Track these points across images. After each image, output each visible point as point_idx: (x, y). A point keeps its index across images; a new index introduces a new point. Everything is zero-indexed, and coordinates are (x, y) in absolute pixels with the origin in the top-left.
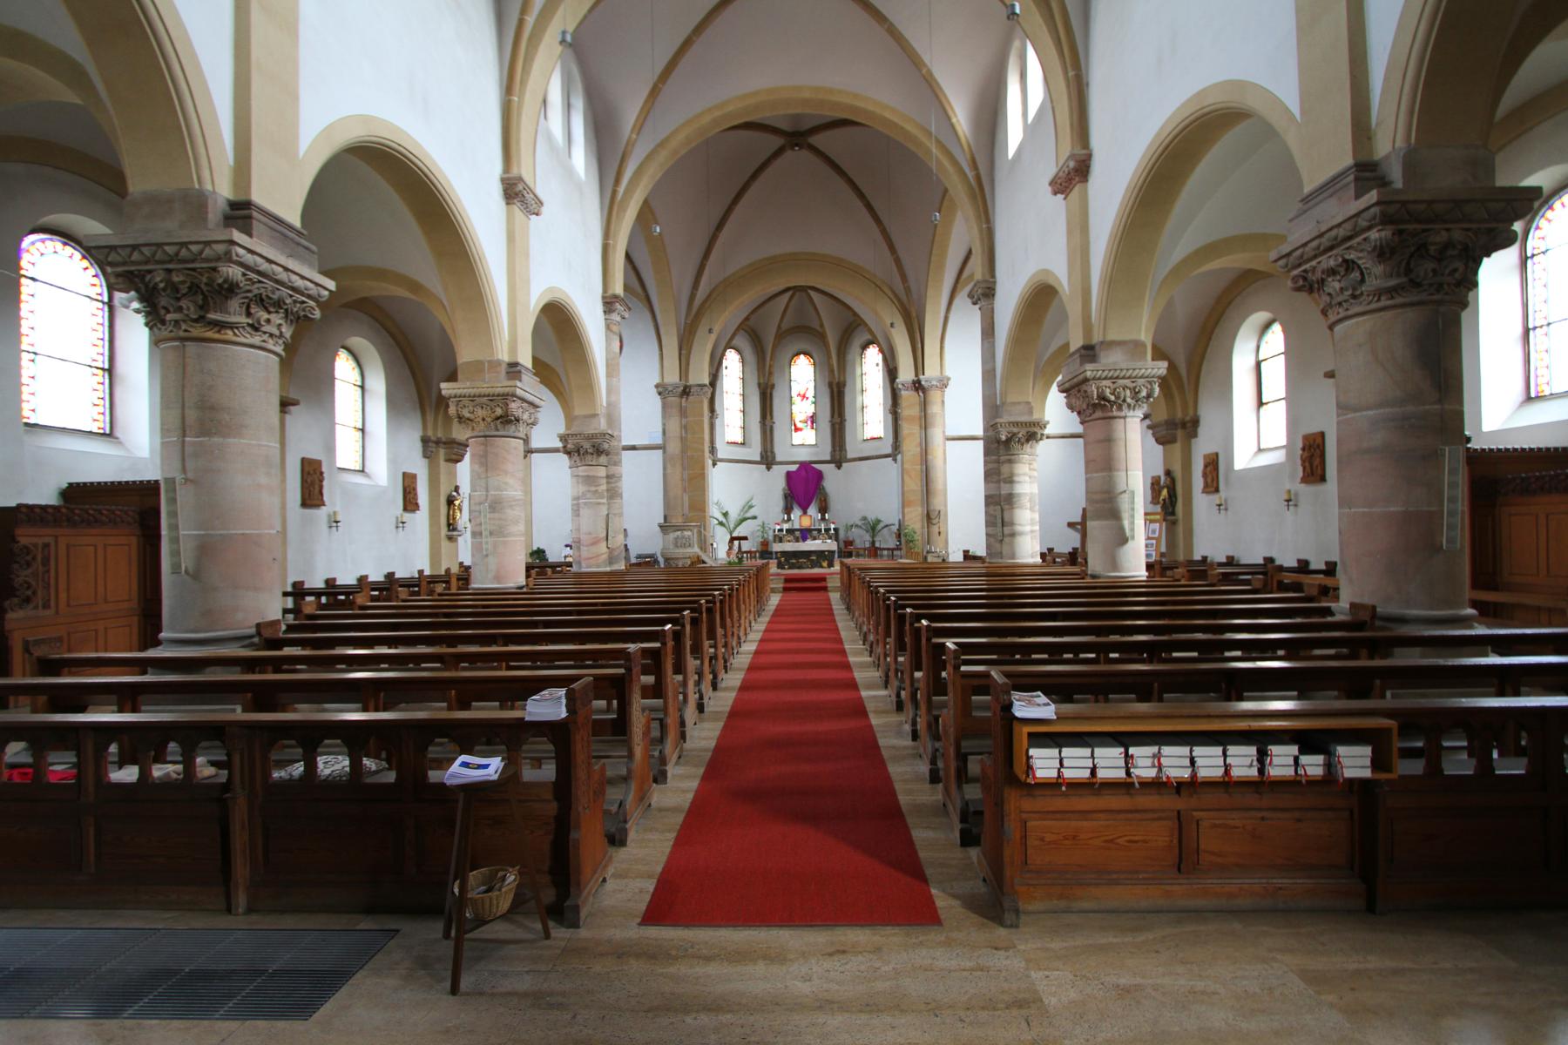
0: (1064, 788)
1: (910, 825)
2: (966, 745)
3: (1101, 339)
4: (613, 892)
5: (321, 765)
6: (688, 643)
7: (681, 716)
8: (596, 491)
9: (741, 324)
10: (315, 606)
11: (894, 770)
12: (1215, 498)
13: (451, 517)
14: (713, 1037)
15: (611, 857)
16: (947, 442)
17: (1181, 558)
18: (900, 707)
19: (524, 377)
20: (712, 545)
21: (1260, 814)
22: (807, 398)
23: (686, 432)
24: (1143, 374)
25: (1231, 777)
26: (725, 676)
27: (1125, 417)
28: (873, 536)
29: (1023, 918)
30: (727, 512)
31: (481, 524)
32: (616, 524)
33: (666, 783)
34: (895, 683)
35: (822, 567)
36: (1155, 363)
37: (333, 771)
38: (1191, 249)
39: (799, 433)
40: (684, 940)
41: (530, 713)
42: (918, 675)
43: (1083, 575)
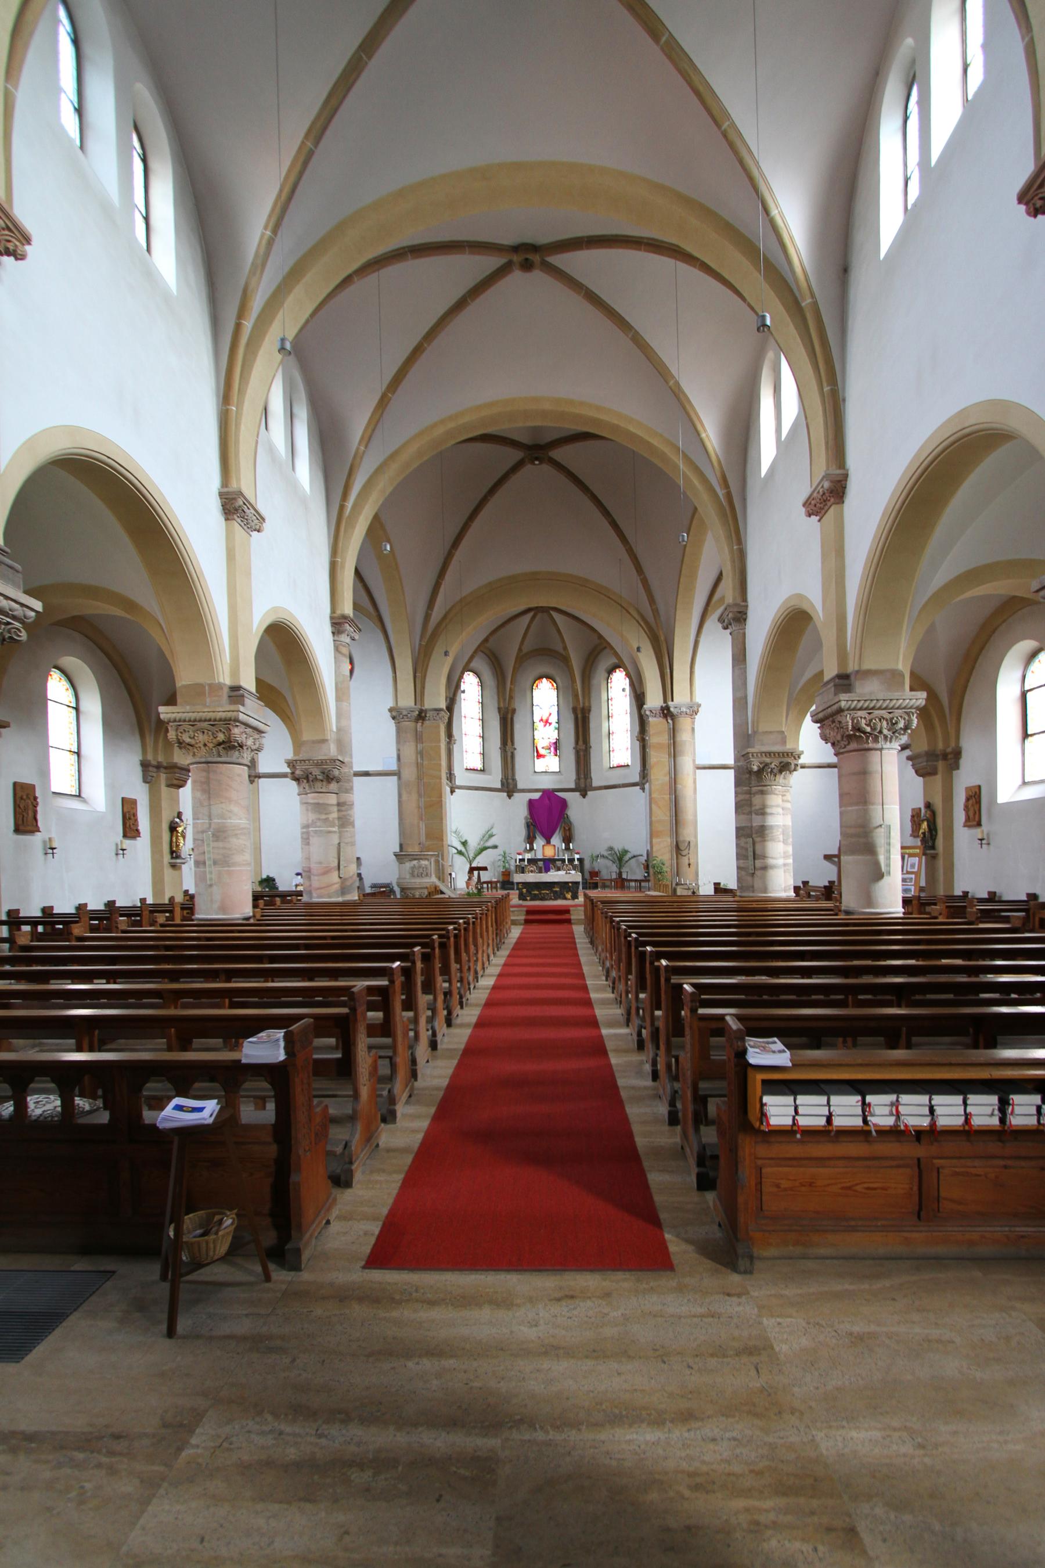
0: (798, 1136)
1: (646, 1168)
2: (703, 1085)
3: (856, 668)
4: (337, 1234)
5: (31, 1105)
6: (419, 979)
7: (412, 1054)
8: (327, 819)
9: (479, 646)
10: (29, 937)
11: (633, 1111)
12: (977, 832)
13: (174, 844)
14: (435, 1382)
15: (335, 1200)
16: (698, 771)
17: (941, 892)
18: (641, 1046)
19: (247, 701)
20: (450, 874)
21: (1002, 1163)
22: (550, 724)
23: (422, 758)
24: (900, 705)
25: (970, 1125)
26: (460, 1012)
27: (881, 750)
28: (620, 867)
29: (758, 1264)
30: (466, 841)
31: (204, 853)
32: (348, 853)
33: (395, 1123)
34: (636, 1022)
35: (566, 899)
36: (913, 693)
37: (44, 1111)
38: (951, 576)
39: (542, 759)
40: (409, 1283)
41: (247, 1056)
42: (658, 1013)
43: (837, 911)
